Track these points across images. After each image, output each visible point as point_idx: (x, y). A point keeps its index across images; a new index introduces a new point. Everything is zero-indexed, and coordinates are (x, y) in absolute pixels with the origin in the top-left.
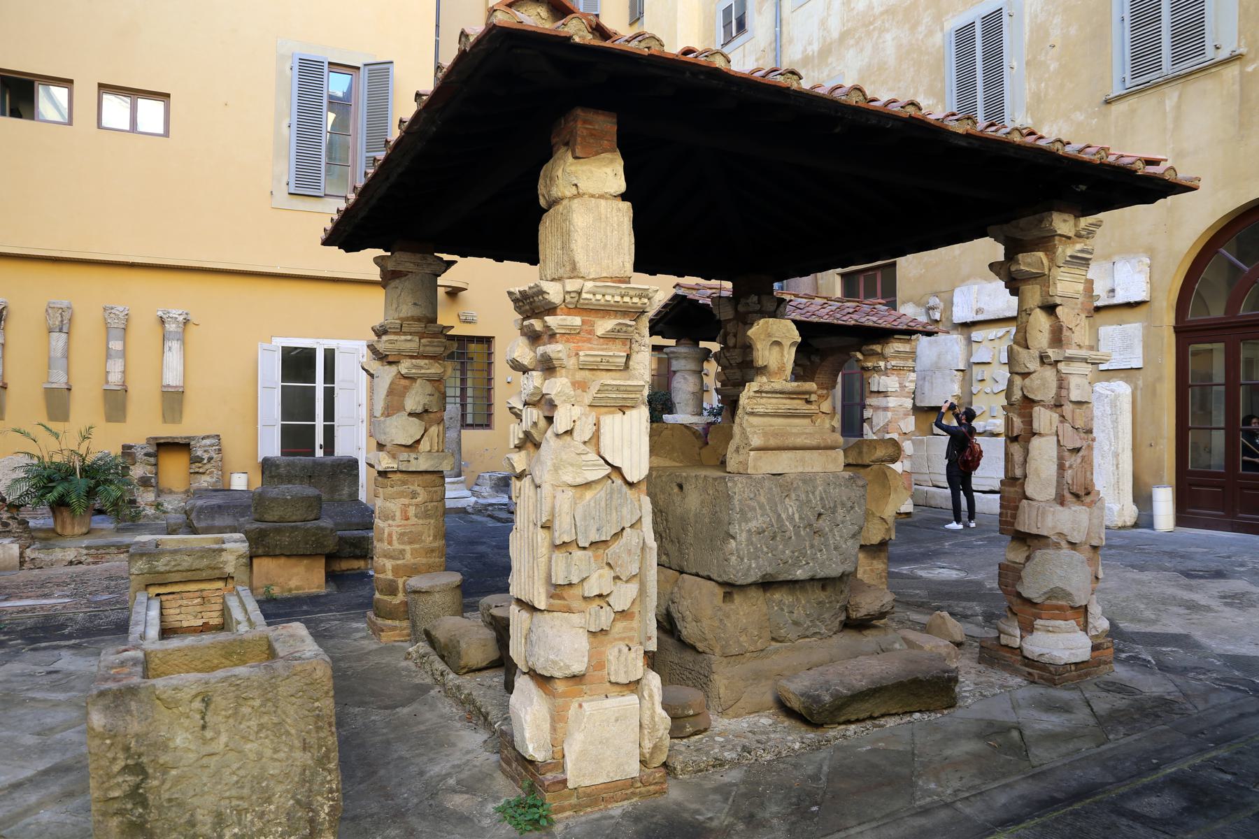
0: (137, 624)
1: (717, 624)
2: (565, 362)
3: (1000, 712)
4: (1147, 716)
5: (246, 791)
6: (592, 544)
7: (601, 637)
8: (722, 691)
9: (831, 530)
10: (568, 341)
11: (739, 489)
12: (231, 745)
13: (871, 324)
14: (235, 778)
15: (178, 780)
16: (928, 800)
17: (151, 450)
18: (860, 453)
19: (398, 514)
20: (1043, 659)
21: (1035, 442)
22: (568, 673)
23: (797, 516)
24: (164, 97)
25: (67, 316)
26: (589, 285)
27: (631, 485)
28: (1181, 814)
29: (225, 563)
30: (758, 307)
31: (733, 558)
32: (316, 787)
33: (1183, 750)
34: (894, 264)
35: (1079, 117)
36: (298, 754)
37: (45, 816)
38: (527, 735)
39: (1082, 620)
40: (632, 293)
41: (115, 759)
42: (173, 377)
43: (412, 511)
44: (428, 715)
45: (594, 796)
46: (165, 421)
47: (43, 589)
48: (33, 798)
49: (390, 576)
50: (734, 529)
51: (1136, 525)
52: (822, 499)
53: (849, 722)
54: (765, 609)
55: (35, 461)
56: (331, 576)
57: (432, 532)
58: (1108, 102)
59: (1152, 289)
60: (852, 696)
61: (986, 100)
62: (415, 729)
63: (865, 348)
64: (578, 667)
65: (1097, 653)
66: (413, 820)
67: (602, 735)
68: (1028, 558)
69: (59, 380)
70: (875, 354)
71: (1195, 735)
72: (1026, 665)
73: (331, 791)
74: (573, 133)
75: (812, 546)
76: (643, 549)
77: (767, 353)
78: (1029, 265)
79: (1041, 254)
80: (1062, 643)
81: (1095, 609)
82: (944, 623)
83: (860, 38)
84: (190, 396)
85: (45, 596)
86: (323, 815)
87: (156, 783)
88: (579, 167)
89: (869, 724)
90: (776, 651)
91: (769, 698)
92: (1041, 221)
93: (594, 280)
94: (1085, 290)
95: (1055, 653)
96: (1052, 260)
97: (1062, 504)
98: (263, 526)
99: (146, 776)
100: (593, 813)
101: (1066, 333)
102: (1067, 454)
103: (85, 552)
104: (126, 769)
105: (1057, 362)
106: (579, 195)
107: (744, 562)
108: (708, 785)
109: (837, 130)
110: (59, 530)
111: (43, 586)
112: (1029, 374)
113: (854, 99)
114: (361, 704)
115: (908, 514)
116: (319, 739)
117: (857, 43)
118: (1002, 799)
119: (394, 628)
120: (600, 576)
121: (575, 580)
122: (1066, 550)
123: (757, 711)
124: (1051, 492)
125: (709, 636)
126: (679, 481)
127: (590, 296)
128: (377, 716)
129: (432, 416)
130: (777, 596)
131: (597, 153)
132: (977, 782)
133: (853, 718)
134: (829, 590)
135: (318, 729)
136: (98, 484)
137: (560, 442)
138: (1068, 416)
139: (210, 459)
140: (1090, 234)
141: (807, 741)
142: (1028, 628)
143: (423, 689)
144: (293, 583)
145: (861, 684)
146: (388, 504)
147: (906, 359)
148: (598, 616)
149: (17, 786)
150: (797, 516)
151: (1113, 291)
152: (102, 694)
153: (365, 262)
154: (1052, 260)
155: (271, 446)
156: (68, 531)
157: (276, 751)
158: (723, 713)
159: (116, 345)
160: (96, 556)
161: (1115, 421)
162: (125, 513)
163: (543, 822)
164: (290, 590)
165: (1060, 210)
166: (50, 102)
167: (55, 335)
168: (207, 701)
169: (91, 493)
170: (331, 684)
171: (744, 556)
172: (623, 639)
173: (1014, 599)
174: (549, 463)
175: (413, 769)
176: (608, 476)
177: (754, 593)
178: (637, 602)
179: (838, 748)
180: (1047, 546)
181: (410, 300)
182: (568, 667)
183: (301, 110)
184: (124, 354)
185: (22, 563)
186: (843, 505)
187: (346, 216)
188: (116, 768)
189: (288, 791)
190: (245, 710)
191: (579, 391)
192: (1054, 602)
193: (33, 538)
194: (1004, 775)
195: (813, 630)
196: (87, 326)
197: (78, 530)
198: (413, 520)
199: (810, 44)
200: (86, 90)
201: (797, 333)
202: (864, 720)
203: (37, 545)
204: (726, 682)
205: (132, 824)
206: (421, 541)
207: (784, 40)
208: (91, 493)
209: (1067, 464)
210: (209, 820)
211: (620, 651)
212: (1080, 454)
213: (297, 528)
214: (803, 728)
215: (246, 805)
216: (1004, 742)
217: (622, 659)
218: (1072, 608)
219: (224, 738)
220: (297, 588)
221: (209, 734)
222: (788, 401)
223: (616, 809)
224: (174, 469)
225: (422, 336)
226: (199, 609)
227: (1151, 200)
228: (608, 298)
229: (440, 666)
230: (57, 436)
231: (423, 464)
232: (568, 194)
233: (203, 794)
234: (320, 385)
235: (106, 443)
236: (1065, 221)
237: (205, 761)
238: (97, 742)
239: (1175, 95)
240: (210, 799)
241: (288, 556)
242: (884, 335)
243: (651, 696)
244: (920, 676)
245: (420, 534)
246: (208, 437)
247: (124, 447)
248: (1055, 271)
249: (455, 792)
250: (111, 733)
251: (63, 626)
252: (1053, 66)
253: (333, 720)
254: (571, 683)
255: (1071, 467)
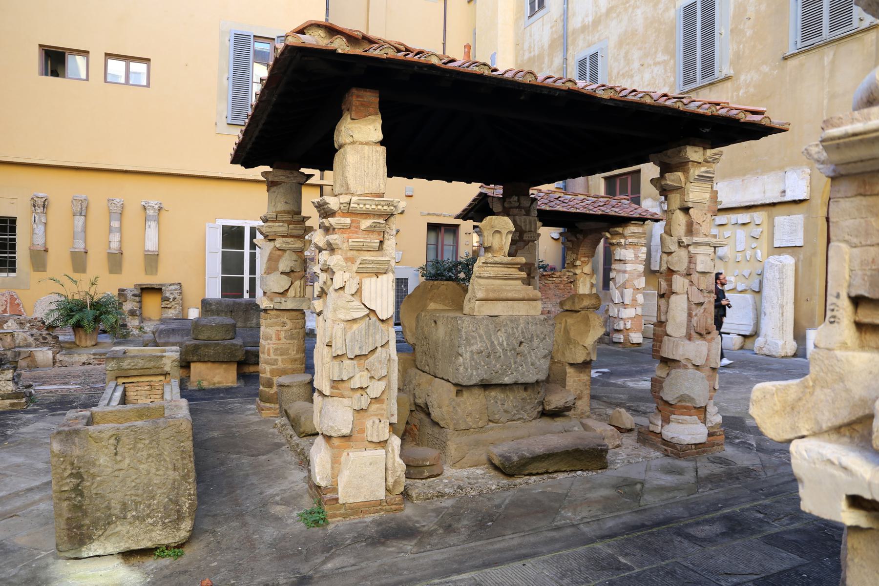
0: (104, 399)
1: (451, 409)
2: (340, 246)
3: (634, 473)
4: (731, 479)
5: (140, 492)
6: (356, 356)
7: (362, 413)
8: (453, 452)
9: (529, 353)
10: (342, 233)
11: (466, 325)
12: (132, 465)
13: (613, 213)
14: (134, 484)
15: (101, 483)
16: (563, 522)
17: (137, 292)
18: (574, 302)
19: (274, 336)
20: (674, 441)
21: (673, 298)
22: (340, 434)
23: (505, 343)
24: (147, 60)
25: (84, 205)
26: (354, 199)
27: (382, 321)
28: (717, 535)
29: (165, 365)
30: (517, 204)
31: (461, 368)
32: (181, 492)
33: (743, 500)
34: (639, 171)
35: (765, 69)
36: (170, 472)
37: (42, 506)
38: (317, 471)
39: (702, 416)
40: (383, 203)
41: (65, 469)
42: (151, 245)
43: (282, 335)
44: (277, 461)
45: (355, 510)
46: (146, 273)
47: (64, 379)
48: (37, 497)
49: (268, 375)
50: (462, 350)
51: (795, 355)
52: (523, 332)
53: (531, 474)
54: (484, 401)
55: (63, 298)
56: (241, 376)
57: (295, 349)
58: (785, 58)
59: (811, 191)
60: (533, 458)
61: (703, 56)
62: (266, 468)
63: (611, 230)
64: (346, 431)
65: (711, 438)
66: (248, 519)
67: (361, 471)
68: (668, 374)
69: (80, 246)
70: (618, 234)
71: (756, 491)
72: (664, 445)
73: (190, 495)
74: (350, 103)
75: (515, 363)
76: (389, 360)
77: (491, 238)
78: (673, 181)
79: (680, 174)
80: (687, 431)
81: (712, 409)
82: (621, 416)
83: (620, 12)
84: (161, 255)
85: (65, 384)
86: (185, 508)
87: (88, 484)
88: (353, 125)
89: (545, 476)
90: (492, 429)
91: (484, 458)
92: (680, 152)
93: (359, 195)
94: (711, 197)
95: (681, 437)
96: (687, 178)
97: (690, 339)
98: (197, 342)
99: (83, 480)
100: (354, 519)
101: (695, 226)
102: (694, 306)
103: (92, 357)
104: (71, 475)
105: (688, 245)
106: (353, 143)
107: (468, 369)
108: (431, 507)
109: (522, 98)
110: (78, 343)
111: (65, 377)
112: (671, 253)
113: (528, 80)
114: (239, 453)
115: (639, 344)
116: (183, 464)
117: (618, 16)
118: (610, 524)
119: (270, 409)
120: (361, 376)
121: (345, 378)
122: (691, 370)
123: (476, 465)
124: (684, 331)
125: (447, 417)
126: (435, 319)
127: (356, 206)
128: (246, 460)
129: (296, 274)
130: (493, 394)
131: (366, 116)
132: (599, 513)
133: (534, 472)
134: (530, 391)
135: (183, 458)
136: (101, 314)
137: (337, 294)
138: (695, 282)
139: (174, 299)
140: (715, 161)
141: (500, 485)
142: (666, 421)
143: (279, 445)
144: (216, 379)
145: (539, 450)
146: (268, 330)
147: (639, 238)
148: (360, 401)
149: (30, 490)
150: (505, 343)
151: (784, 192)
152: (59, 433)
153: (257, 172)
154: (687, 178)
155: (214, 291)
156: (83, 343)
157: (158, 470)
158: (454, 465)
159: (115, 224)
160: (99, 360)
161: (782, 283)
162: (120, 333)
163: (321, 522)
164: (214, 384)
165: (694, 145)
166: (76, 64)
167: (77, 217)
168: (118, 440)
169: (97, 320)
170: (191, 433)
171: (468, 367)
172: (377, 415)
173: (659, 401)
174: (331, 307)
175: (257, 491)
176: (368, 315)
177: (476, 391)
178: (386, 393)
179: (521, 490)
180: (679, 367)
181: (283, 200)
182: (340, 430)
183: (236, 68)
184: (120, 230)
185: (54, 363)
186: (538, 336)
187: (240, 147)
188: (66, 474)
189: (164, 493)
190: (140, 446)
191: (349, 264)
192: (684, 404)
193: (61, 347)
194: (618, 510)
195: (518, 416)
196: (97, 211)
197: (89, 343)
198: (283, 340)
199: (587, 16)
200: (97, 58)
201: (512, 225)
202: (542, 474)
203: (64, 352)
204: (455, 446)
205: (75, 506)
206: (288, 354)
207: (569, 14)
208: (97, 320)
209: (694, 313)
210: (119, 506)
211: (374, 422)
212: (703, 306)
213: (218, 344)
214: (501, 476)
215: (140, 500)
216: (630, 489)
217: (375, 427)
218: (695, 408)
219: (127, 461)
220: (219, 383)
221: (119, 458)
222: (506, 269)
223: (369, 518)
224: (152, 304)
225: (289, 223)
226: (148, 393)
227: (757, 138)
228: (368, 206)
229: (291, 432)
230: (76, 282)
231: (290, 305)
232: (348, 141)
233: (115, 492)
234: (247, 250)
235: (106, 286)
236: (696, 152)
237: (116, 473)
238: (56, 459)
239: (831, 53)
240: (119, 495)
241: (213, 362)
242: (624, 221)
243: (393, 451)
244: (581, 447)
245: (288, 349)
246: (173, 284)
247: (119, 290)
248: (689, 185)
249: (278, 504)
250: (64, 455)
251: (72, 402)
252: (749, 33)
253: (192, 454)
254: (343, 440)
255: (696, 315)
